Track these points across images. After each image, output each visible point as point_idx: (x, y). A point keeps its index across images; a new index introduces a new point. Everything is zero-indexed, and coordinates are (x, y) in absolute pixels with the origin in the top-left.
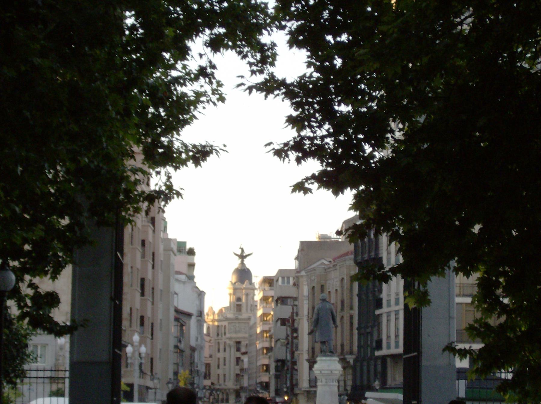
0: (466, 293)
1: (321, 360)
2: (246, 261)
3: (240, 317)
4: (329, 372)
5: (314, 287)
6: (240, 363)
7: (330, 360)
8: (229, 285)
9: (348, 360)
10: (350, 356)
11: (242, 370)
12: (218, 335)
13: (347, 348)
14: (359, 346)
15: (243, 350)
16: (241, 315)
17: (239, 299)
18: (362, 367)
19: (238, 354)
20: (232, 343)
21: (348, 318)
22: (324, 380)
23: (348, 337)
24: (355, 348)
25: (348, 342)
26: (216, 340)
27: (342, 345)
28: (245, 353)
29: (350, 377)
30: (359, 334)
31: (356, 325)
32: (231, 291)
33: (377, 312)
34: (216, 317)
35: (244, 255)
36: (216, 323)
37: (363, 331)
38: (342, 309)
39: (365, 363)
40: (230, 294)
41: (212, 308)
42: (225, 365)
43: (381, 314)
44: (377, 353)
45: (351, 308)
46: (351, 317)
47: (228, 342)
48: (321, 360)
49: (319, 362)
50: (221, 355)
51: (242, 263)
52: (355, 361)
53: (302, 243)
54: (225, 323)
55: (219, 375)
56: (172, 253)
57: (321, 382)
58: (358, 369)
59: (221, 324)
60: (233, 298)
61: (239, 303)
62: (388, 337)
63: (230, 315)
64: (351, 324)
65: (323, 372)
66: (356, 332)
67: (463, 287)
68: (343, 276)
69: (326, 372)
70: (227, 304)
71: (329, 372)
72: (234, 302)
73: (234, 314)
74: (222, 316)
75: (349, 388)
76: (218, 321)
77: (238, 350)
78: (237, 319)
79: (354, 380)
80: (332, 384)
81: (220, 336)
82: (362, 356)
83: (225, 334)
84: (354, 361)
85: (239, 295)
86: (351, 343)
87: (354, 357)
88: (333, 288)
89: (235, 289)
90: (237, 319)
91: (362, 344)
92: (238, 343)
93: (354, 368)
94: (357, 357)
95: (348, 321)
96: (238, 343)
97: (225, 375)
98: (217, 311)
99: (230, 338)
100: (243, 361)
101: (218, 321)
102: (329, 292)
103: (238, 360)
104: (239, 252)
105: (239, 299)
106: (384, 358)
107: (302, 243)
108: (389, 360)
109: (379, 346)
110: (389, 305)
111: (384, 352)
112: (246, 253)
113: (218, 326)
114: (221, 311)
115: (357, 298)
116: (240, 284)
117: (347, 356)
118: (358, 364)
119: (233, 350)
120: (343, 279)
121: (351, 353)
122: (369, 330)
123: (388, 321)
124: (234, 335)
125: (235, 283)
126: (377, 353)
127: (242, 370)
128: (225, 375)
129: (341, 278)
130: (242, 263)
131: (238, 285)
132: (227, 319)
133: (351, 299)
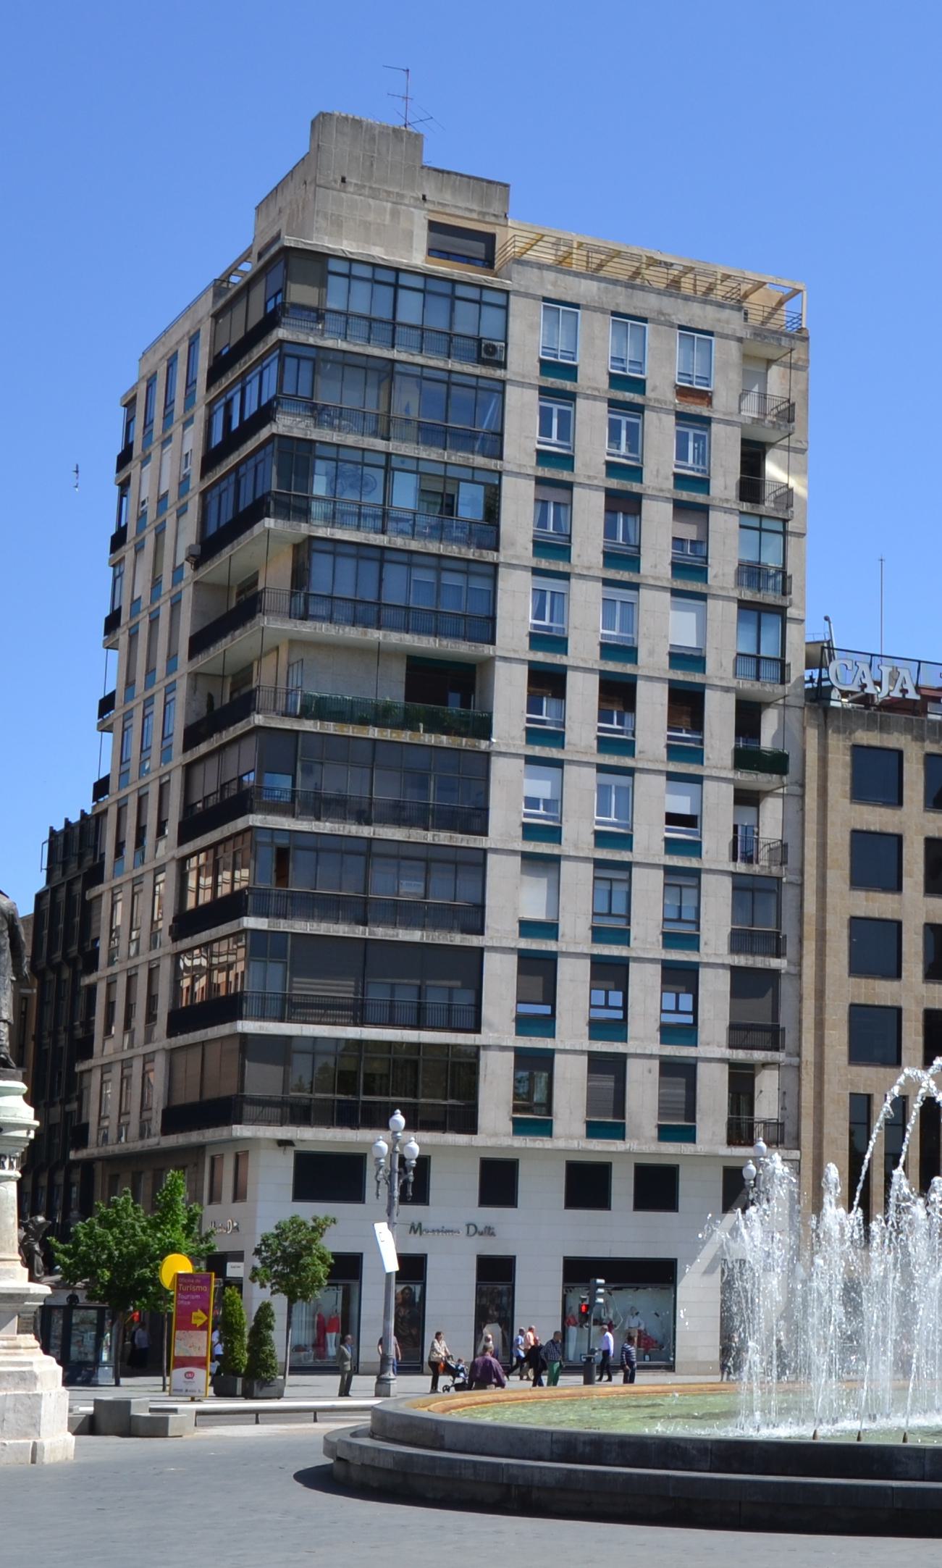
43: (100, 896)
111: (83, 1154)
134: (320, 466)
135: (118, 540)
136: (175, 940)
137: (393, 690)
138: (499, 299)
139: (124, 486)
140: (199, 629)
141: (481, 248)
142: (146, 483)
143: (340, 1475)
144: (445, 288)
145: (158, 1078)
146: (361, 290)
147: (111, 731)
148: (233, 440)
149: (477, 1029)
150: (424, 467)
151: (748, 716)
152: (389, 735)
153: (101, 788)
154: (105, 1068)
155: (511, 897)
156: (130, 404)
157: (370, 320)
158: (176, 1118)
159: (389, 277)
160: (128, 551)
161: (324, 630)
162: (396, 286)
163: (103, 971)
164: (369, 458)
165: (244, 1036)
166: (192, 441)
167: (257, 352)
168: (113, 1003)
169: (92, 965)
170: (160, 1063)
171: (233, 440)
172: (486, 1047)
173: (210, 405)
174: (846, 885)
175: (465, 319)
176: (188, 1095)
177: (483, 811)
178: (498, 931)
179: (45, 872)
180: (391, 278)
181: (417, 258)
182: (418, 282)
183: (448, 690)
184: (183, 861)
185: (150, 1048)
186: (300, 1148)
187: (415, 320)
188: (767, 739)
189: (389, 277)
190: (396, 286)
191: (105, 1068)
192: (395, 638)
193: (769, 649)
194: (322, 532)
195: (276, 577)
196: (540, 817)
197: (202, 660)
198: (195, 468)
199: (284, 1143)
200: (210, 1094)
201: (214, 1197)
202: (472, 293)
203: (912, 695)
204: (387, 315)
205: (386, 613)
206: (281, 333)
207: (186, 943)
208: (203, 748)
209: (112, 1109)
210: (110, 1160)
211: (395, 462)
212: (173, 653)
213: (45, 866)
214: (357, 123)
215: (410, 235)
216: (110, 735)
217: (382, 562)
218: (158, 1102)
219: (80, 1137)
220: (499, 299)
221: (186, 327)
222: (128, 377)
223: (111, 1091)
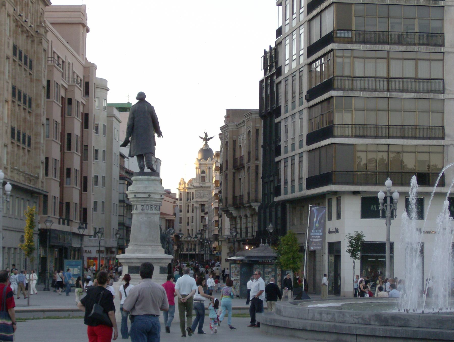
0: (357, 134)
1: (136, 180)
2: (209, 143)
3: (204, 185)
4: (146, 196)
5: (227, 142)
6: (203, 220)
7: (148, 180)
8: (195, 161)
9: (253, 207)
10: (255, 204)
11: (205, 226)
12: (188, 200)
13: (252, 197)
14: (264, 195)
15: (206, 210)
16: (205, 184)
17: (203, 172)
18: (265, 213)
19: (203, 214)
20: (198, 205)
21: (254, 168)
22: (140, 207)
23: (254, 187)
24: (260, 196)
25: (254, 190)
26: (186, 203)
27: (249, 194)
28: (206, 213)
29: (256, 224)
30: (264, 183)
31: (261, 175)
32: (197, 166)
33: (277, 159)
34: (186, 186)
35: (208, 138)
36: (187, 191)
37: (266, 180)
38: (249, 161)
39: (268, 210)
40: (197, 168)
41: (183, 179)
42: (192, 222)
43: (280, 161)
44: (277, 199)
45: (257, 159)
46: (257, 167)
47: (195, 205)
48: (136, 180)
49: (134, 182)
50: (190, 215)
51: (206, 144)
52: (260, 208)
53: (228, 111)
54: (193, 190)
55: (188, 230)
56: (114, 119)
57: (136, 209)
58: (262, 215)
59: (189, 191)
60: (199, 171)
61: (203, 175)
62: (286, 183)
63: (196, 184)
64: (257, 173)
65: (138, 196)
66: (261, 181)
67: (355, 127)
68: (249, 130)
69: (142, 196)
70: (194, 176)
71: (146, 196)
72: (199, 175)
73: (199, 183)
74: (191, 185)
75: (255, 234)
76: (188, 189)
77: (203, 211)
78: (201, 187)
79: (259, 227)
80: (150, 212)
81: (189, 201)
82: (266, 203)
83: (193, 199)
84: (258, 208)
85: (203, 169)
86: (256, 191)
87: (259, 204)
88: (243, 142)
89: (200, 164)
90: (201, 187)
91: (266, 192)
92: (203, 205)
93: (259, 214)
94: (262, 204)
95: (254, 171)
96: (203, 205)
97: (192, 230)
98: (187, 182)
99: (196, 202)
100: (205, 219)
101: (188, 189)
102: (240, 146)
103: (203, 217)
104: (203, 136)
105: (203, 172)
106: (283, 203)
107: (228, 111)
108: (288, 205)
109: (277, 192)
110: (286, 152)
111: (282, 197)
112: (209, 136)
113: (188, 193)
114: (190, 181)
115: (262, 149)
116: (204, 160)
117: (252, 204)
118: (262, 211)
119: (199, 211)
120: (249, 132)
121: (256, 201)
122: (271, 179)
123: (285, 167)
124: (199, 200)
125: (200, 160)
126: (277, 199)
127: (205, 226)
128: (192, 230)
129: (248, 131)
130: (206, 144)
131: (203, 161)
132: (194, 187)
133: (257, 149)
136: (308, 101)
138: (440, 57)
140: (310, 132)
147: (281, 5)
149: (443, 138)
153: (279, 32)
158: (313, 182)
163: (283, 156)
164: (380, 149)
168: (287, 180)
169: (278, 153)
172: (448, 146)
178: (450, 90)
179: (263, 70)
184: (310, 64)
185: (301, 151)
186: (365, 195)
199: (355, 193)
200: (324, 172)
201: (330, 218)
208: (315, 13)
210: (291, 201)
212: (301, 92)
213: (263, 68)
216: (281, 7)
218: (305, 175)
220: (440, 57)
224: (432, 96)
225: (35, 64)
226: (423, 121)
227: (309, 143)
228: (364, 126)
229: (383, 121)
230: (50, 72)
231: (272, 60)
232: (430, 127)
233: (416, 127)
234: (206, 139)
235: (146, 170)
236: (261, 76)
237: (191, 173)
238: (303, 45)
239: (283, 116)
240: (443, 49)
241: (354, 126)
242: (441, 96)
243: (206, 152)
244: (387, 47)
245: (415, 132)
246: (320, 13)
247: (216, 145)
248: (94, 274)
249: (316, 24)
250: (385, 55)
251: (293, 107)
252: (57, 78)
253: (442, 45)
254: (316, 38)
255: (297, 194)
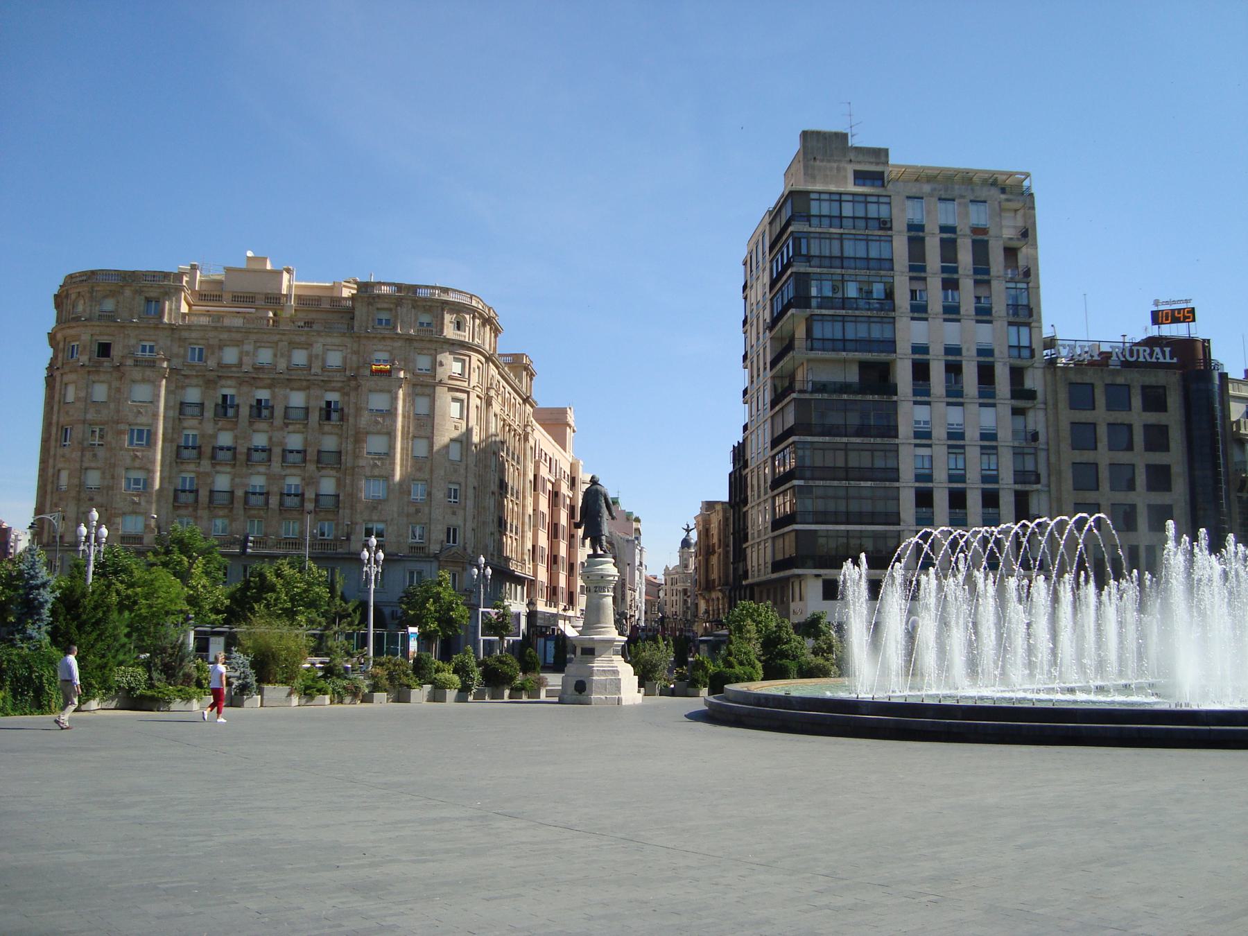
63: (680, 570)
106: (752, 586)
111: (750, 581)
134: (813, 283)
135: (745, 322)
137: (853, 376)
139: (745, 298)
141: (877, 178)
142: (752, 295)
143: (695, 717)
144: (862, 199)
145: (769, 551)
146: (825, 205)
148: (780, 275)
150: (859, 278)
151: (1017, 374)
152: (852, 397)
153: (745, 428)
154: (752, 546)
155: (908, 465)
156: (745, 264)
157: (830, 217)
159: (837, 197)
160: (748, 326)
161: (820, 354)
162: (840, 201)
165: (796, 531)
166: (766, 279)
167: (784, 238)
170: (769, 544)
171: (780, 275)
173: (771, 261)
174: (1106, 448)
175: (873, 211)
176: (779, 557)
177: (896, 428)
180: (839, 197)
181: (851, 188)
182: (850, 198)
183: (878, 378)
187: (851, 214)
188: (1028, 384)
189: (837, 197)
190: (840, 201)
191: (752, 546)
192: (851, 355)
193: (1025, 342)
194: (818, 312)
195: (801, 332)
196: (922, 428)
197: (775, 371)
198: (767, 289)
199: (817, 576)
202: (874, 199)
203: (1096, 358)
204: (837, 214)
205: (848, 345)
206: (790, 229)
207: (776, 492)
208: (777, 408)
209: (755, 564)
210: (759, 584)
211: (846, 278)
214: (51, 368)
215: (845, 177)
217: (843, 322)
219: (745, 575)
221: (760, 230)
222: (744, 253)
223: (755, 555)
224: (887, 484)
225: (1153, 699)
226: (880, 507)
227: (773, 531)
228: (825, 513)
229: (842, 508)
230: (537, 467)
231: (739, 453)
232: (886, 514)
233: (873, 514)
234: (688, 531)
235: (600, 552)
236: (731, 469)
237: (674, 561)
238: (768, 440)
239: (749, 505)
240: (897, 441)
241: (815, 513)
242: (896, 484)
243: (686, 543)
244: (845, 440)
245: (872, 518)
246: (782, 409)
247: (694, 537)
248: (784, 655)
249: (779, 420)
250: (843, 446)
251: (759, 497)
252: (544, 472)
253: (897, 437)
254: (779, 432)
255: (763, 578)
